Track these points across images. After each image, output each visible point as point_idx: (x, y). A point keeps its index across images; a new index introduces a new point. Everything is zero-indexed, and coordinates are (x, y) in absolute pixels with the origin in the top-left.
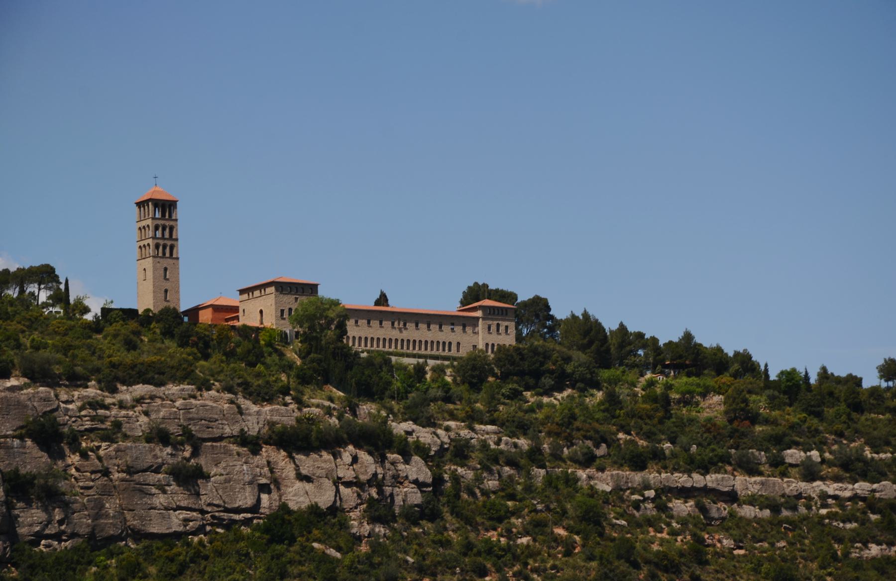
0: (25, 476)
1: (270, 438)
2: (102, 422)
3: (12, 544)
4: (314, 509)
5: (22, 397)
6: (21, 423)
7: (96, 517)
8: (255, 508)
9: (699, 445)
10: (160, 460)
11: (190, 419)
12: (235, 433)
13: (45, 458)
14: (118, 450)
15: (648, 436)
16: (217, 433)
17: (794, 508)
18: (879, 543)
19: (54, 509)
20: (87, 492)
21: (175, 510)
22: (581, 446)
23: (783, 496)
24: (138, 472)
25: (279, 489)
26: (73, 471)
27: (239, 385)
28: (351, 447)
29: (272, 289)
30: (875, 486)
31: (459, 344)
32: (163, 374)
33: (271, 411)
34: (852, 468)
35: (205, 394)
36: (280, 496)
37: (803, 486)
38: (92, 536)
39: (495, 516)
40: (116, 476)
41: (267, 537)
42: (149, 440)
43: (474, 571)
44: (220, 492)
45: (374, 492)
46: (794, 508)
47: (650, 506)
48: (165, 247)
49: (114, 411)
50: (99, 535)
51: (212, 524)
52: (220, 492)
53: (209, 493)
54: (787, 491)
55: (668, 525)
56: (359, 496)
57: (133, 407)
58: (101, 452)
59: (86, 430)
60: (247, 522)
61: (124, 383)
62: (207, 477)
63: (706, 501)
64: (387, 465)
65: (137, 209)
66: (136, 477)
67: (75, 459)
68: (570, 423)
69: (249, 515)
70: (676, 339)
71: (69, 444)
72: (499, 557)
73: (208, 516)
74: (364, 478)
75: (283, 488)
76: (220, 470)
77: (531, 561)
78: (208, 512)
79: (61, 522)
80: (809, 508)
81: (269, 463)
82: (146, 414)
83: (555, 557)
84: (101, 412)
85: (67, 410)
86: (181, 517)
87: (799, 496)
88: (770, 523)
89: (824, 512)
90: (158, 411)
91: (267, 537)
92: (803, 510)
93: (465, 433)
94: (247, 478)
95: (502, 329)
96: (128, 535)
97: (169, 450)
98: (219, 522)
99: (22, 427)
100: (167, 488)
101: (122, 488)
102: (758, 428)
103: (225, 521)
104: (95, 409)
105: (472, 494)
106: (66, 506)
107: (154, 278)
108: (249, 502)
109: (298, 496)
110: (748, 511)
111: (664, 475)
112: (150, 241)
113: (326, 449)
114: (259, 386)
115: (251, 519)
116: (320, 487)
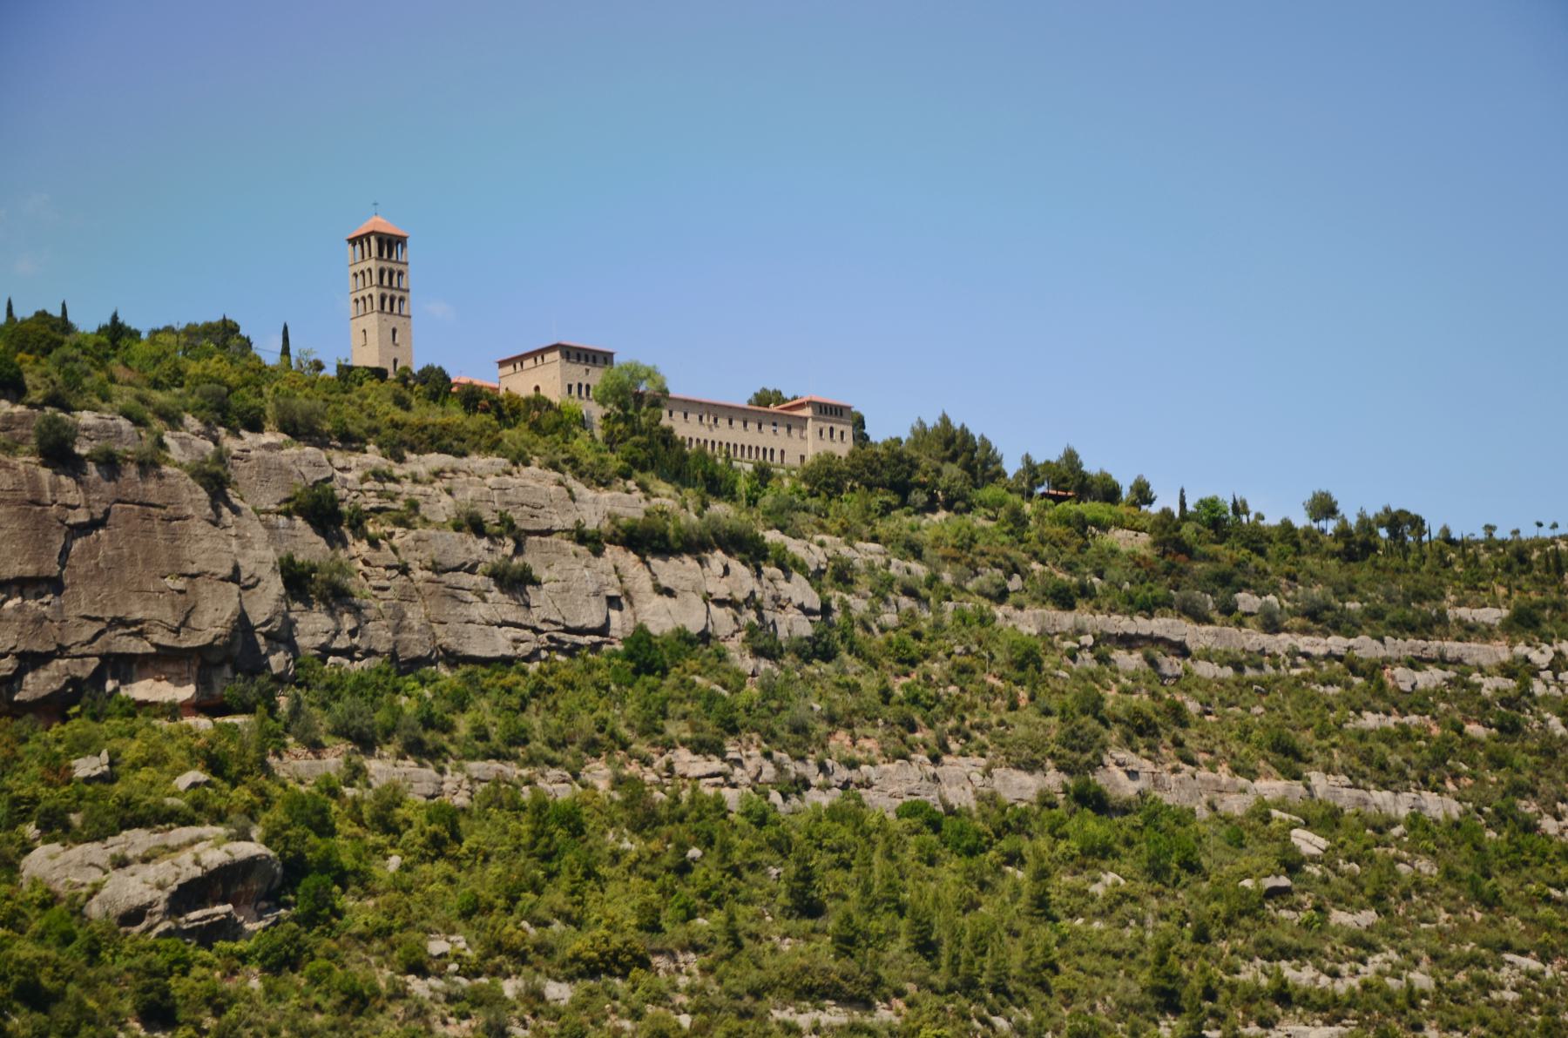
0: (302, 565)
1: (615, 535)
2: (393, 500)
3: (295, 659)
4: (682, 636)
5: (284, 460)
6: (286, 495)
7: (398, 630)
8: (603, 630)
9: (1132, 583)
10: (474, 557)
11: (508, 503)
12: (568, 526)
13: (321, 544)
14: (418, 540)
15: (1069, 567)
16: (544, 524)
17: (1260, 667)
18: (1376, 712)
19: (342, 614)
20: (381, 595)
21: (500, 626)
22: (990, 576)
23: (1243, 650)
24: (447, 571)
25: (631, 604)
26: (360, 565)
27: (565, 461)
28: (719, 553)
29: (557, 355)
30: (1352, 641)
31: (782, 452)
32: (463, 440)
33: (612, 499)
34: (1317, 617)
35: (525, 470)
36: (635, 615)
37: (1266, 640)
38: (394, 655)
39: (907, 657)
40: (418, 574)
41: (632, 665)
42: (458, 528)
43: (902, 724)
44: (558, 604)
45: (751, 615)
46: (1260, 667)
47: (1088, 656)
48: (392, 300)
49: (407, 486)
50: (403, 655)
51: (549, 649)
52: (558, 604)
53: (544, 604)
54: (1248, 646)
55: (1116, 681)
56: (735, 619)
57: (432, 482)
58: (396, 541)
59: (372, 510)
60: (595, 648)
61: (412, 450)
62: (537, 583)
63: (1157, 654)
64: (765, 581)
65: (350, 247)
66: (445, 577)
67: (363, 547)
68: (970, 547)
69: (597, 639)
70: (1054, 459)
71: (351, 527)
72: (929, 708)
73: (543, 637)
74: (740, 596)
75: (636, 603)
76: (554, 575)
77: (967, 715)
78: (542, 632)
79: (353, 633)
80: (1276, 667)
81: (616, 568)
82: (449, 492)
83: (996, 711)
84: (390, 486)
85: (345, 480)
86: (509, 636)
87: (1262, 652)
88: (1237, 684)
89: (1296, 672)
90: (464, 490)
91: (632, 665)
92: (1269, 670)
93: (845, 551)
94: (592, 587)
95: (836, 434)
96: (438, 659)
97: (485, 542)
98: (559, 647)
99: (287, 501)
100: (487, 595)
101: (428, 591)
102: (1198, 566)
103: (567, 642)
104: (382, 482)
105: (868, 629)
106: (357, 610)
107: (380, 341)
108: (596, 621)
109: (660, 617)
110: (1205, 669)
111: (1099, 617)
112: (375, 292)
113: (689, 553)
114: (591, 464)
115: (599, 644)
116: (686, 604)
